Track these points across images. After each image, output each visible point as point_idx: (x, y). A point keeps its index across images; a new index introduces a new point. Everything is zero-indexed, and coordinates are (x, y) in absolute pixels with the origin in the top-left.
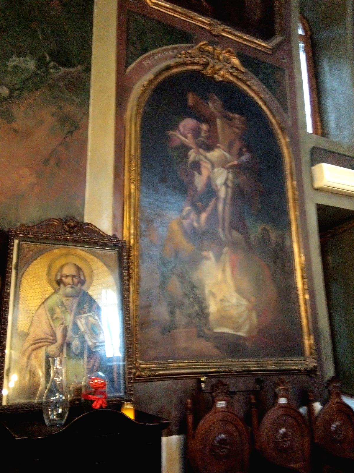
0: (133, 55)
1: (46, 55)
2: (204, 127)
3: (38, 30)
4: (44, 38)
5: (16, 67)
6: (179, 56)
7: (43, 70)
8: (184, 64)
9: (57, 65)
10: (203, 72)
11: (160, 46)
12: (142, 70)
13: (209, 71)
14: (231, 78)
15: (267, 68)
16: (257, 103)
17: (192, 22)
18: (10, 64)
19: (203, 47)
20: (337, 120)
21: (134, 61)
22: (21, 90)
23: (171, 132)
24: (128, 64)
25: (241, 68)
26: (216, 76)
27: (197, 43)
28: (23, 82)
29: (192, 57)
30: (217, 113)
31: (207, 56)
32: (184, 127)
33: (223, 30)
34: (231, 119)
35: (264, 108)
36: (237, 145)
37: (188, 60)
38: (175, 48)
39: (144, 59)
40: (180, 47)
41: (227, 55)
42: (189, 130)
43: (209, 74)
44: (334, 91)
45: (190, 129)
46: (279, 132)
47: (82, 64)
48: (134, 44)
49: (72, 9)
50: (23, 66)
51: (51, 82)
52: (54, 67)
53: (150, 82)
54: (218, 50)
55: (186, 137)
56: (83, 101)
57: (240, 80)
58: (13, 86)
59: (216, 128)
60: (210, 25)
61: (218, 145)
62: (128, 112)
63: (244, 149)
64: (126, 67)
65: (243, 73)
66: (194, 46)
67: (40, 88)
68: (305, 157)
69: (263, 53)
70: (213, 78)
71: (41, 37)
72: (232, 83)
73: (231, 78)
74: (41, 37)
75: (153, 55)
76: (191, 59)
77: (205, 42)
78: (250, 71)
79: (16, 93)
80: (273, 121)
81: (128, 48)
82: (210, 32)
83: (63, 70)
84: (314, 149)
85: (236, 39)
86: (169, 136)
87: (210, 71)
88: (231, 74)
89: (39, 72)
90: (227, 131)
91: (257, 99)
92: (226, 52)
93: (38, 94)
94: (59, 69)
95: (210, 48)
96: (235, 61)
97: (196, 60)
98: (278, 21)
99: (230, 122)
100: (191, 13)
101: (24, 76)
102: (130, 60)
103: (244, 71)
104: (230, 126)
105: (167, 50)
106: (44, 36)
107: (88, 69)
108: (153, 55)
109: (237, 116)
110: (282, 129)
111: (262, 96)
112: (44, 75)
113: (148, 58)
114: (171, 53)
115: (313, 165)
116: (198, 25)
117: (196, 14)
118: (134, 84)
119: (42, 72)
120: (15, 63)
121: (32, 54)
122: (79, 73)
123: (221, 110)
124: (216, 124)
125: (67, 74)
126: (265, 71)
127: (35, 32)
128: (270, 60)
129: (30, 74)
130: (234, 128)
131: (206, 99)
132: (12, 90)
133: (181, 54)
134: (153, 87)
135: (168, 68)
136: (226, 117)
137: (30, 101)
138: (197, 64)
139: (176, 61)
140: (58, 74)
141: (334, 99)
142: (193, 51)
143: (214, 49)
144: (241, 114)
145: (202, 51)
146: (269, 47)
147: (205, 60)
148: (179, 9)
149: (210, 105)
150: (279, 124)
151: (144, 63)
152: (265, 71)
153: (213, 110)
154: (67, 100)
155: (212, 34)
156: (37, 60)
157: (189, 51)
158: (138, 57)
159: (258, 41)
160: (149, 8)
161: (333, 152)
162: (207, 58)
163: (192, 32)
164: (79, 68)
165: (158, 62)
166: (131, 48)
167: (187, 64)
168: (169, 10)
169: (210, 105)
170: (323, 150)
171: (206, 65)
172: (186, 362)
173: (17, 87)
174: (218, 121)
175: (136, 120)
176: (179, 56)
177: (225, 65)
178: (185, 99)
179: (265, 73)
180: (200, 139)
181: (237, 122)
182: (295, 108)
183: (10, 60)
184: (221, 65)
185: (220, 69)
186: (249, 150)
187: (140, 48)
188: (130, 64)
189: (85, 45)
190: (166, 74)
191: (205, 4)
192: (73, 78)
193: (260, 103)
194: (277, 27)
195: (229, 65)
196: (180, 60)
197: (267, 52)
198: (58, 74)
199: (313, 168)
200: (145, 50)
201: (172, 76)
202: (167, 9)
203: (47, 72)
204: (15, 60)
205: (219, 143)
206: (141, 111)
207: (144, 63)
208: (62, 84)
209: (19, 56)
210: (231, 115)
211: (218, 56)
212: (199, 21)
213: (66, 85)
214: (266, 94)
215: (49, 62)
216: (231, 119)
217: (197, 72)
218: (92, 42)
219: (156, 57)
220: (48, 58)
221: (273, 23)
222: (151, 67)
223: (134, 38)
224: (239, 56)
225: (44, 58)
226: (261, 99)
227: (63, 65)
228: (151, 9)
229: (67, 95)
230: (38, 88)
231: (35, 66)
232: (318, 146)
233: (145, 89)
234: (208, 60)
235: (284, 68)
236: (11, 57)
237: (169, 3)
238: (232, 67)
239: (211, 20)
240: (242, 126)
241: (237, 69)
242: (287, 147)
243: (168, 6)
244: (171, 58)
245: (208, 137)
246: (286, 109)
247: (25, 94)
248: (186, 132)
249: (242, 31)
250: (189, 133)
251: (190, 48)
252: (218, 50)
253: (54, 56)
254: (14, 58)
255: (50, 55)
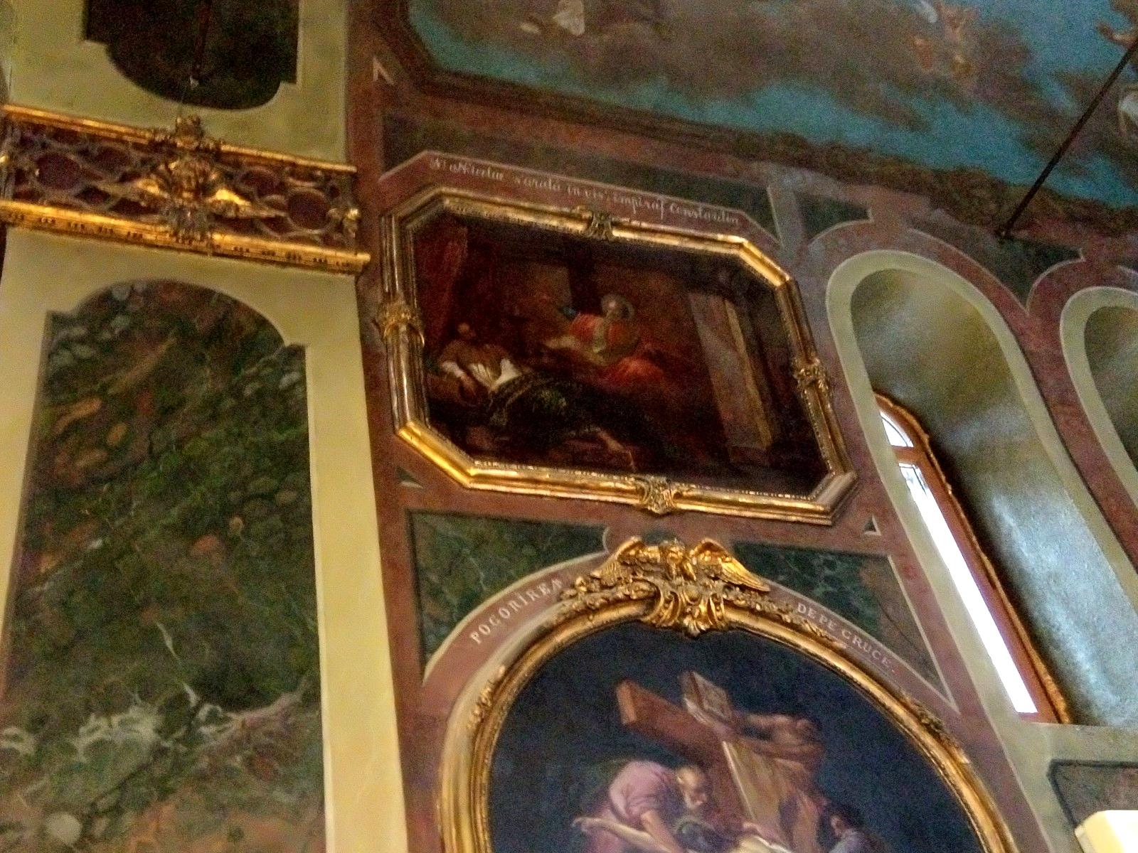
0: (437, 622)
1: (188, 689)
2: (688, 778)
3: (160, 626)
4: (177, 647)
5: (99, 746)
6: (570, 592)
7: (180, 733)
8: (588, 611)
9: (219, 708)
10: (648, 618)
11: (511, 580)
12: (469, 659)
13: (663, 612)
14: (733, 616)
15: (831, 565)
16: (834, 670)
17: (585, 497)
18: (83, 741)
19: (632, 552)
20: (1101, 657)
21: (441, 638)
22: (116, 811)
23: (589, 821)
24: (425, 651)
25: (755, 582)
26: (686, 621)
27: (613, 548)
28: (122, 786)
29: (604, 587)
30: (720, 728)
31: (648, 573)
32: (626, 794)
33: (678, 496)
34: (765, 735)
35: (858, 677)
36: (808, 810)
37: (598, 599)
38: (554, 575)
39: (472, 627)
40: (567, 568)
41: (706, 558)
42: (643, 799)
43: (670, 620)
44: (1054, 577)
45: (649, 796)
46: (928, 739)
47: (292, 689)
48: (436, 593)
49: (254, 549)
50: (120, 737)
51: (204, 763)
52: (213, 718)
53: (498, 686)
54: (676, 551)
55: (639, 826)
56: (303, 795)
57: (763, 615)
58: (93, 805)
59: (726, 772)
60: (640, 492)
61: (747, 825)
62: (446, 792)
63: (835, 821)
64: (423, 662)
65: (762, 593)
66: (606, 557)
67: (173, 791)
68: (1043, 804)
69: (808, 526)
70: (679, 628)
71: (169, 643)
72: (742, 628)
73: (733, 616)
74: (169, 643)
75: (493, 609)
76: (607, 593)
77: (634, 539)
78: (782, 583)
79: (101, 825)
80: (899, 711)
81: (420, 607)
82: (644, 510)
83: (237, 720)
84: (1058, 771)
85: (719, 511)
86: (583, 835)
87: (666, 614)
88: (729, 604)
89: (167, 744)
90: (764, 774)
91: (827, 656)
92: (701, 552)
93: (167, 809)
94: (227, 720)
95: (652, 552)
96: (733, 568)
97: (620, 592)
98: (823, 438)
99: (764, 745)
100: (580, 476)
101: (128, 765)
102: (431, 639)
103: (766, 589)
104: (770, 755)
105: (533, 585)
106: (179, 639)
107: (312, 699)
108: (493, 609)
109: (781, 720)
110: (933, 730)
111: (841, 645)
112: (182, 749)
113: (482, 618)
114: (544, 590)
115: (1075, 824)
116: (607, 502)
117: (594, 474)
118: (453, 704)
119: (178, 740)
120: (97, 736)
121: (146, 696)
122: (287, 716)
123: (725, 716)
124: (724, 761)
125: (249, 729)
126: (828, 572)
127: (151, 635)
128: (836, 541)
129: (145, 757)
130: (780, 761)
131: (674, 694)
132: (87, 822)
133: (573, 586)
134: (507, 697)
135: (544, 634)
136: (748, 731)
137: (144, 838)
138: (628, 600)
139: (565, 610)
140: (224, 736)
141: (1066, 601)
142: (610, 569)
143: (664, 551)
144: (795, 711)
145: (631, 564)
146: (821, 509)
147: (645, 586)
148: (546, 474)
149: (691, 706)
150: (918, 718)
151: (474, 636)
152: (828, 572)
153: (703, 719)
154: (253, 806)
155: (651, 513)
156: (160, 711)
157: (597, 574)
158: (452, 626)
159: (786, 501)
160: (468, 492)
161: (1124, 766)
162: (650, 579)
163: (592, 522)
164: (285, 700)
165: (512, 625)
166: (430, 607)
167: (597, 611)
168: (515, 483)
169: (691, 706)
170: (1086, 764)
171: (651, 599)
172: (527, 205)
173: (103, 804)
174: (728, 749)
175: (472, 809)
176: (570, 592)
177: (706, 587)
178: (611, 704)
179: (827, 579)
180: (686, 818)
181: (787, 738)
182: (952, 659)
183: (82, 730)
184: (694, 591)
185: (695, 600)
186: (852, 818)
187: (455, 601)
188: (433, 651)
189: (298, 632)
190: (541, 652)
191: (614, 445)
192: (270, 734)
193: (842, 666)
194: (826, 451)
195: (719, 584)
196: (576, 605)
197: (815, 521)
198: (224, 736)
199: (1079, 832)
200: (470, 601)
201: (562, 653)
202: (511, 483)
203: (192, 739)
204: (96, 729)
205: (749, 819)
206: (484, 778)
207: (474, 636)
208: (237, 761)
209: (108, 711)
210: (761, 721)
211: (680, 566)
212: (608, 489)
213: (249, 762)
214: (849, 636)
215: (197, 708)
216: (765, 735)
217: (633, 621)
218: (315, 619)
219: (505, 613)
220: (193, 698)
221: (811, 447)
222: (492, 644)
223: (434, 578)
224: (743, 554)
225: (182, 698)
226: (842, 654)
227: (236, 704)
228: (473, 492)
229: (256, 789)
230: (165, 794)
231: (158, 731)
232: (1069, 757)
233: (486, 713)
234: (651, 584)
235: (880, 552)
236: (81, 723)
237: (514, 466)
238: (729, 586)
239: (639, 479)
240: (807, 748)
241: (743, 588)
242: (969, 782)
243: (513, 474)
244: (549, 602)
245: (709, 809)
246: (925, 665)
247: (128, 819)
248: (635, 810)
249: (730, 486)
250: (644, 810)
251: (597, 563)
252: (676, 551)
253: (211, 688)
254: (93, 721)
255: (197, 686)
